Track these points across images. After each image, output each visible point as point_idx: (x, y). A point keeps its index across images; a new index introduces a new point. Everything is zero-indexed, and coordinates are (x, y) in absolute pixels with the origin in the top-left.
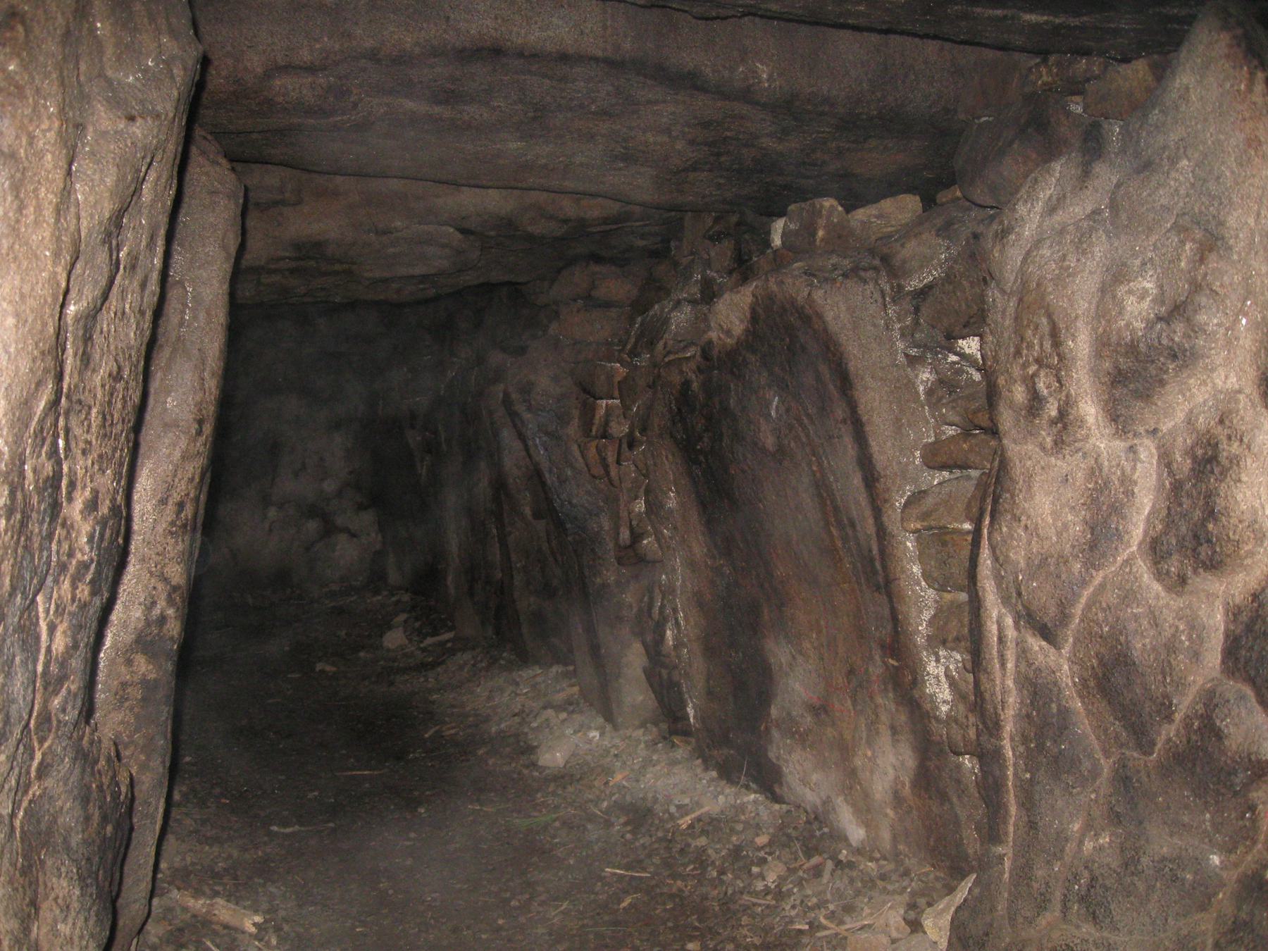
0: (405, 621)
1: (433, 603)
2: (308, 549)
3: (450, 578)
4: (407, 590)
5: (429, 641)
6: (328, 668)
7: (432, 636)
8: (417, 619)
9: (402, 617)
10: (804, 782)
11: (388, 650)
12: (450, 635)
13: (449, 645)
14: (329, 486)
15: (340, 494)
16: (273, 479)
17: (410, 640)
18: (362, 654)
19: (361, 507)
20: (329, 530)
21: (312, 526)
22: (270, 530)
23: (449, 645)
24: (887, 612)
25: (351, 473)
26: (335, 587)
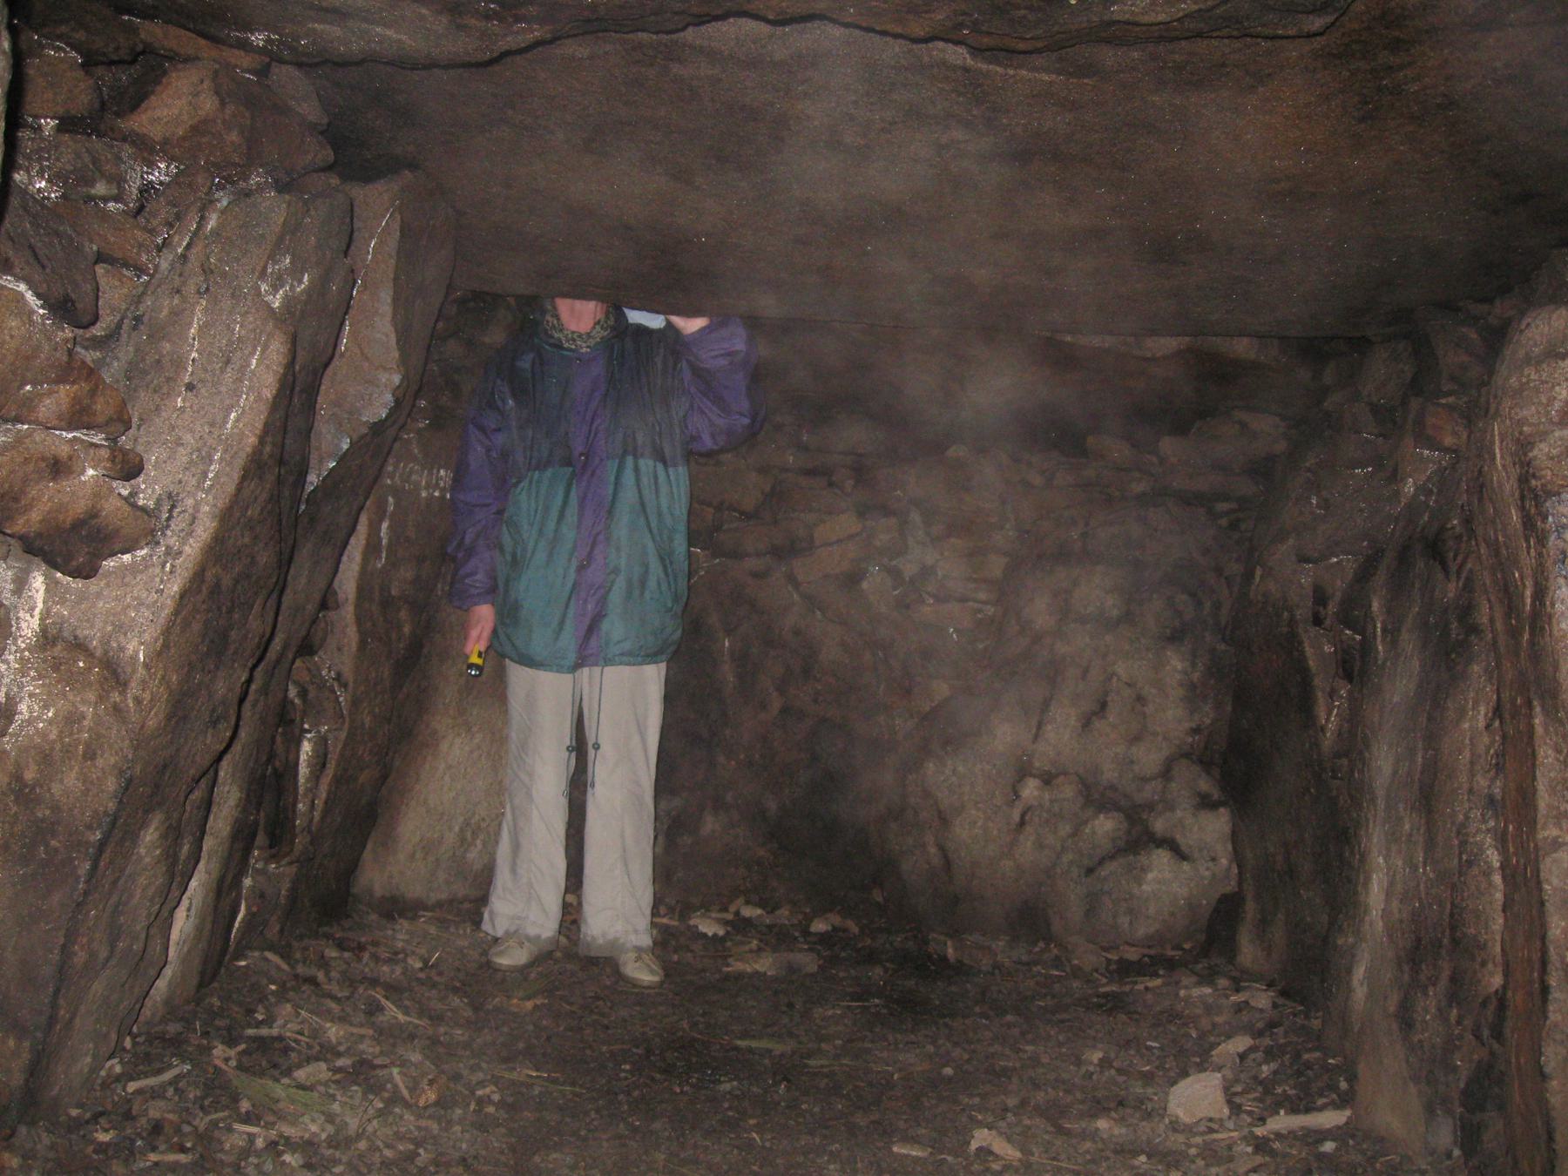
0: (1242, 1057)
1: (1316, 1023)
2: (1090, 871)
3: (1359, 972)
4: (1270, 985)
5: (1282, 1122)
6: (1002, 1147)
7: (1294, 1110)
8: (1270, 1054)
9: (1241, 1043)
10: (1306, 631)
11: (1175, 1126)
12: (1330, 1119)
13: (1329, 1146)
14: (1150, 758)
15: (1166, 773)
16: (1039, 726)
17: (1236, 1109)
18: (1102, 1124)
19: (1206, 803)
20: (1139, 839)
21: (1105, 826)
22: (1022, 823)
23: (1329, 1146)
24: (1536, 956)
25: (1196, 731)
26: (1132, 954)
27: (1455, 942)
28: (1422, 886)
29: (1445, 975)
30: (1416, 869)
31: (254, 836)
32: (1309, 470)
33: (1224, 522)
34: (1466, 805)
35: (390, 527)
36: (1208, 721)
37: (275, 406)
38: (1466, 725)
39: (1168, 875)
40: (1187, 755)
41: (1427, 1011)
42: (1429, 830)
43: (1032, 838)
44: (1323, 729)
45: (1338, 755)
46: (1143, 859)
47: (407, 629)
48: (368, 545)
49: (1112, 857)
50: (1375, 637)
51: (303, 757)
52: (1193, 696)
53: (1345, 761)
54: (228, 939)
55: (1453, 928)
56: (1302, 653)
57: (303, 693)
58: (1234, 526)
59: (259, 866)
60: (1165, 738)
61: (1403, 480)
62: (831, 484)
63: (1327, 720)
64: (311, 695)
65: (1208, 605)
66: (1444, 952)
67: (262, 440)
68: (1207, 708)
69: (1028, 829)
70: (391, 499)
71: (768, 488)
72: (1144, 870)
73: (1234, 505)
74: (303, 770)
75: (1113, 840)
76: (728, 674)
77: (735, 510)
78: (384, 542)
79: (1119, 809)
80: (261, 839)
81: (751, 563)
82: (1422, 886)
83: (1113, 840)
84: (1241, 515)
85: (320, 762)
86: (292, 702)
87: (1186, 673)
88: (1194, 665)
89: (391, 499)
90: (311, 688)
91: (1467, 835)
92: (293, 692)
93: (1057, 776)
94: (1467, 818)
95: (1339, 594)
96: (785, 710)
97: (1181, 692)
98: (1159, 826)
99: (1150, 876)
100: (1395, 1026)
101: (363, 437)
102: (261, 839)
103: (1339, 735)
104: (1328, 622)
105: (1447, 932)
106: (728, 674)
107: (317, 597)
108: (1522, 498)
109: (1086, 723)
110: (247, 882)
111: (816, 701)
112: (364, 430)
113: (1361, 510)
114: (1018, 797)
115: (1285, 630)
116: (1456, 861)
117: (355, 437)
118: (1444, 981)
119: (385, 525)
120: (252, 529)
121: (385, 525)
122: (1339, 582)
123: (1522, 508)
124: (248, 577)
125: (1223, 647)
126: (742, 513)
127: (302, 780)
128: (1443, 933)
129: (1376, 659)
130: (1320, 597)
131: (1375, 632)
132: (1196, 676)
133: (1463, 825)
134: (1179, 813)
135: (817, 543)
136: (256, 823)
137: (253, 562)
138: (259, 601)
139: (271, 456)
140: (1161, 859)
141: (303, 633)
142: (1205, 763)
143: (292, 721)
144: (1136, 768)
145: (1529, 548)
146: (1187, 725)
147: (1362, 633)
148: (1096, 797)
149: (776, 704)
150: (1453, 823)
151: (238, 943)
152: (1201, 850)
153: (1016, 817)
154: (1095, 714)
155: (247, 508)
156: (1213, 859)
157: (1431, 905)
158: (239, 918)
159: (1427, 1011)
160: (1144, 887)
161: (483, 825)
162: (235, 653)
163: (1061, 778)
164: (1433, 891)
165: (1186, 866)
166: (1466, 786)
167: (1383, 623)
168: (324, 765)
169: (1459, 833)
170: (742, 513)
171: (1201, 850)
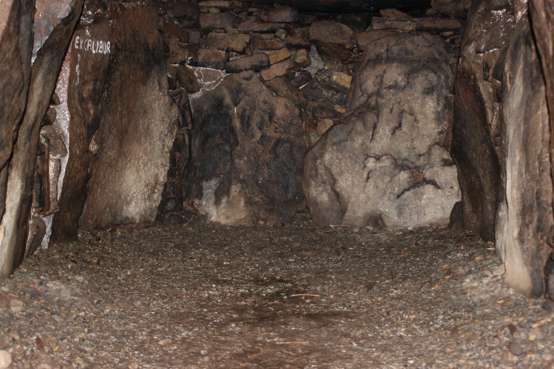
15: (429, 152)
19: (446, 163)
20: (418, 182)
21: (404, 176)
22: (368, 178)
25: (440, 133)
27: (539, 204)
28: (525, 183)
29: (536, 218)
30: (522, 176)
31: (31, 202)
32: (480, 13)
33: (448, 41)
34: (541, 146)
35: (79, 67)
36: (446, 128)
37: (13, 9)
38: (540, 112)
39: (432, 196)
40: (438, 143)
41: (529, 235)
42: (527, 158)
43: (373, 184)
44: (490, 125)
45: (497, 136)
46: (421, 189)
47: (92, 112)
48: (70, 76)
49: (408, 190)
50: (506, 81)
51: (51, 169)
52: (439, 119)
53: (499, 138)
54: (25, 246)
55: (538, 198)
56: (480, 92)
57: (48, 141)
58: (453, 42)
59: (36, 215)
60: (427, 137)
61: (517, 12)
62: (275, 37)
63: (492, 121)
64: (51, 142)
65: (443, 77)
66: (534, 209)
67: (8, 24)
68: (445, 122)
69: (371, 180)
70: (79, 55)
71: (248, 41)
72: (422, 194)
73: (451, 33)
74: (51, 174)
75: (408, 182)
76: (237, 123)
77: (234, 52)
78: (78, 74)
79: (409, 169)
80: (34, 204)
81: (245, 74)
82: (525, 183)
83: (408, 182)
84: (455, 37)
85: (58, 171)
86: (43, 145)
87: (435, 108)
88: (438, 104)
89: (79, 55)
90: (51, 138)
91: (542, 159)
92: (43, 141)
93: (382, 156)
94: (541, 151)
95: (493, 66)
96: (263, 137)
97: (433, 116)
98: (428, 175)
99: (425, 197)
100: (517, 243)
101: (59, 25)
102: (34, 204)
103: (497, 127)
104: (490, 78)
105: (536, 201)
106: (237, 123)
107: (48, 97)
108: (545, 6)
109: (393, 132)
110: (31, 222)
111: (276, 132)
112: (59, 22)
113: (502, 28)
114: (365, 167)
115: (472, 83)
116: (538, 171)
117: (56, 25)
118: (535, 223)
119: (77, 67)
120: (9, 63)
121: (77, 67)
122: (494, 60)
123: (546, 11)
124: (10, 83)
125: (451, 95)
126: (238, 52)
127: (51, 178)
128: (534, 201)
129: (507, 91)
130: (486, 67)
131: (506, 79)
132: (440, 109)
133: (541, 155)
134: (435, 169)
135: (271, 63)
136: (32, 196)
137: (11, 77)
138: (16, 95)
139: (14, 31)
140: (429, 188)
141: (44, 113)
142: (444, 146)
143: (44, 153)
144: (416, 150)
145: (549, 27)
146: (437, 131)
147: (501, 80)
148: (400, 165)
149: (258, 135)
150: (536, 155)
151: (29, 250)
152: (446, 184)
153: (365, 176)
154: (396, 128)
155: (5, 54)
156: (452, 188)
157: (528, 190)
158: (29, 237)
159: (529, 235)
160: (423, 201)
161: (135, 195)
162: (8, 117)
163: (384, 157)
164: (529, 184)
165: (440, 191)
166: (541, 138)
167: (510, 74)
168: (60, 171)
169: (538, 158)
170: (238, 52)
171: (446, 184)
